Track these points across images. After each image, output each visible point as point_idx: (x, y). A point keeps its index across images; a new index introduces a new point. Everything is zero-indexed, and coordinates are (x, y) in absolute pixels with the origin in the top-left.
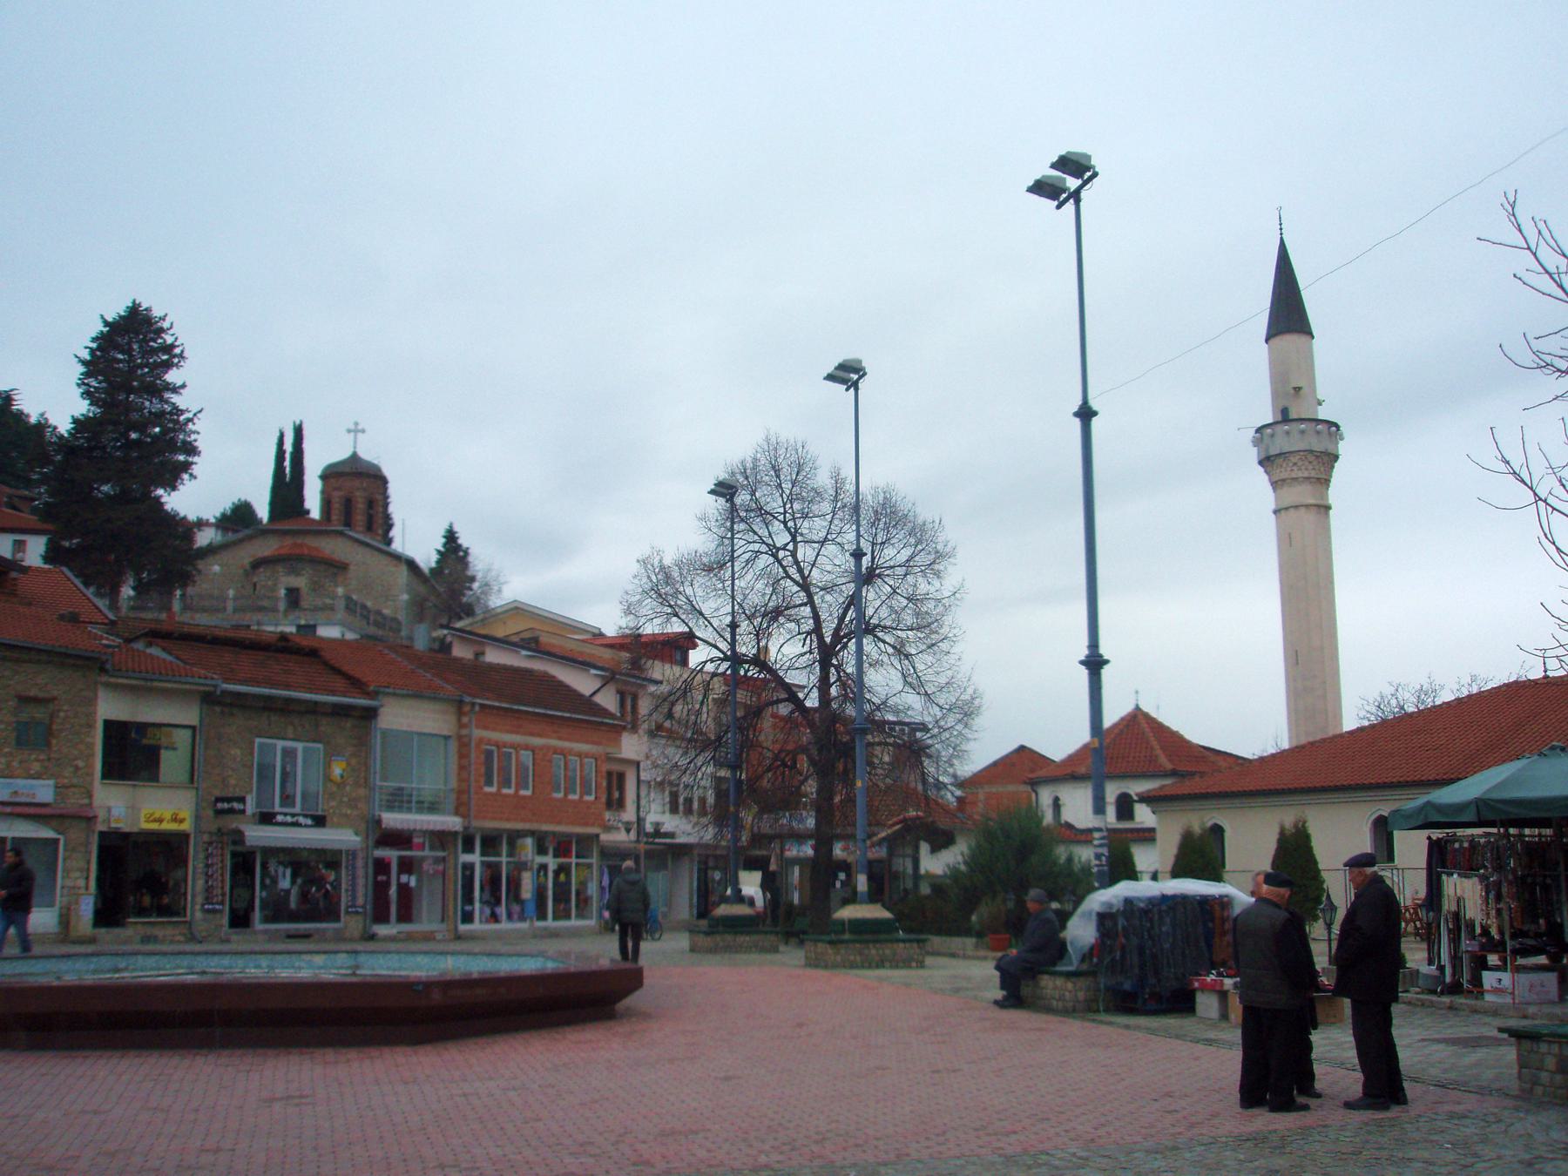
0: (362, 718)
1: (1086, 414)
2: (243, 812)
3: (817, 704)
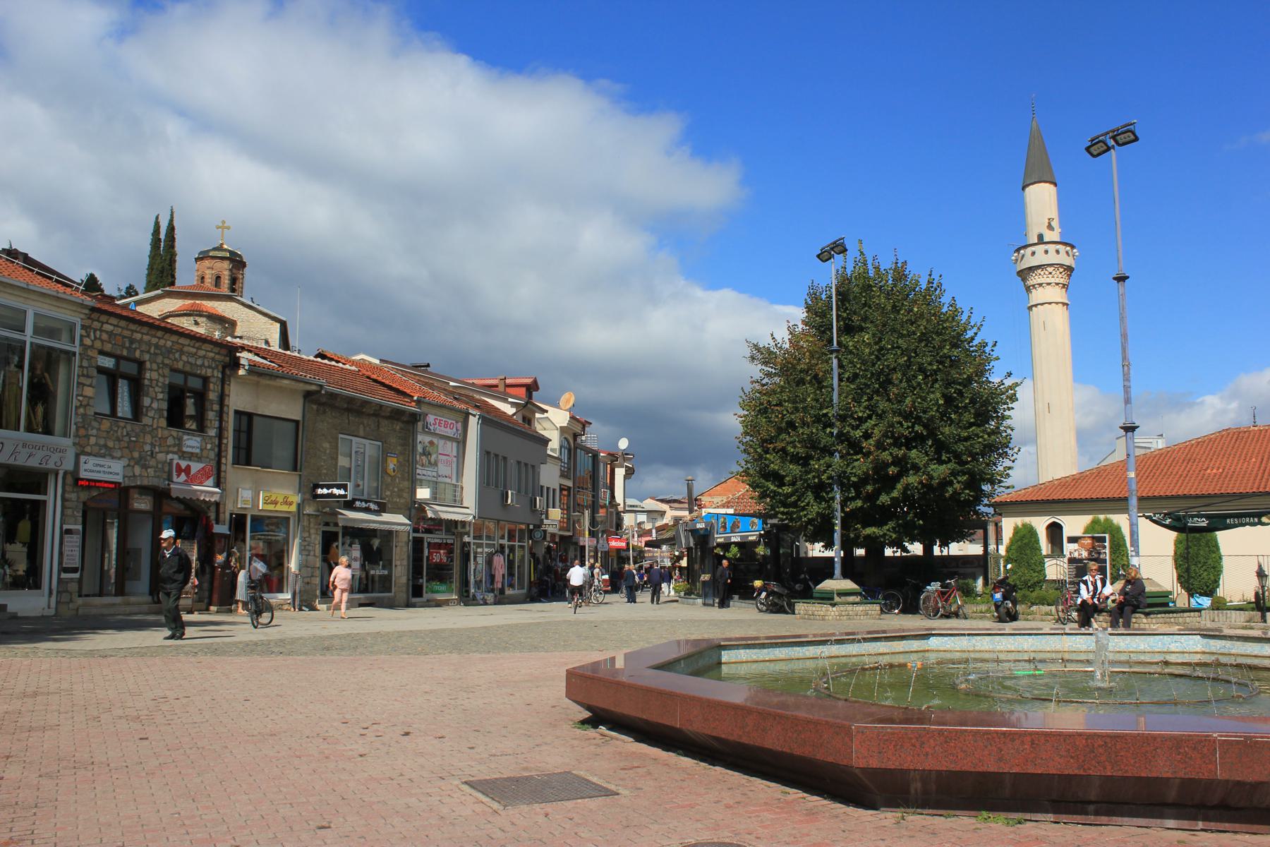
0: (407, 422)
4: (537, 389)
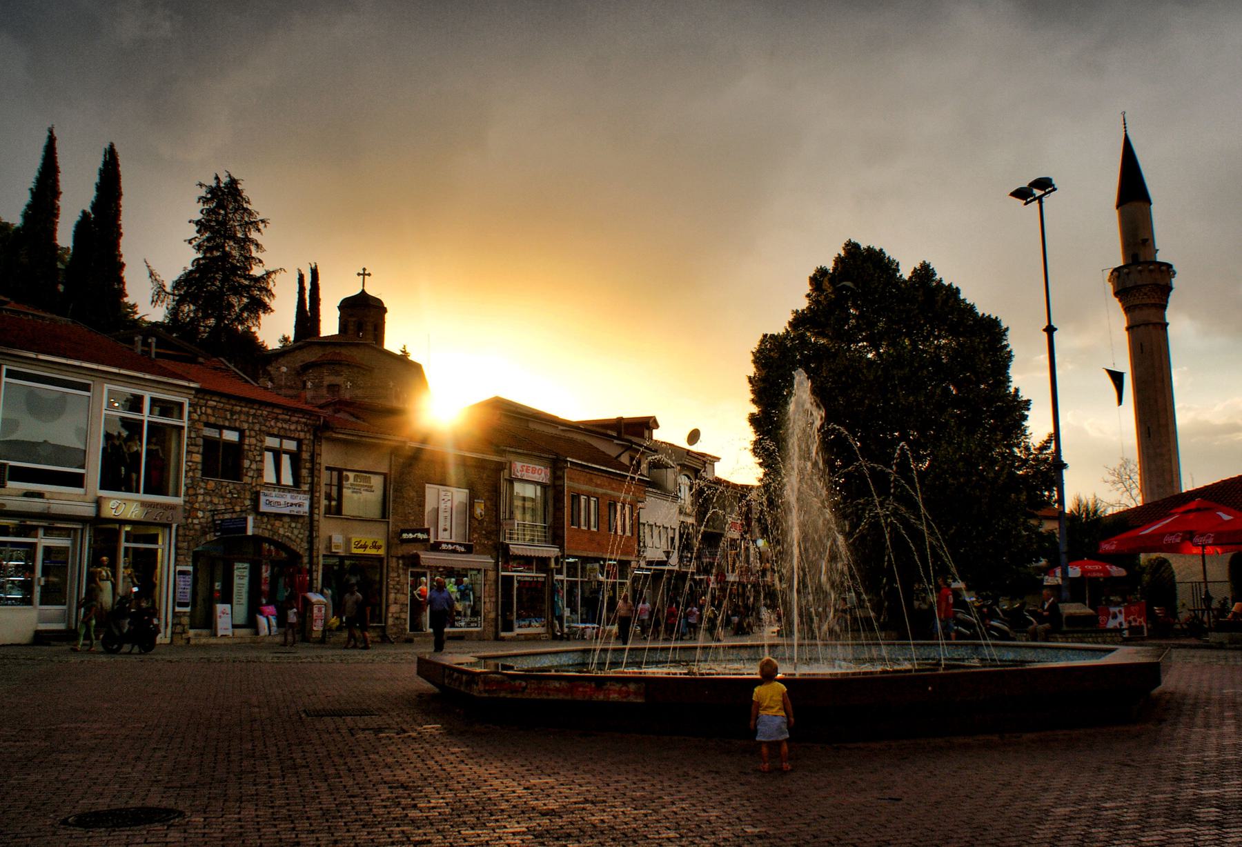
1: (1050, 330)
2: (428, 540)
3: (237, 565)
4: (657, 426)
